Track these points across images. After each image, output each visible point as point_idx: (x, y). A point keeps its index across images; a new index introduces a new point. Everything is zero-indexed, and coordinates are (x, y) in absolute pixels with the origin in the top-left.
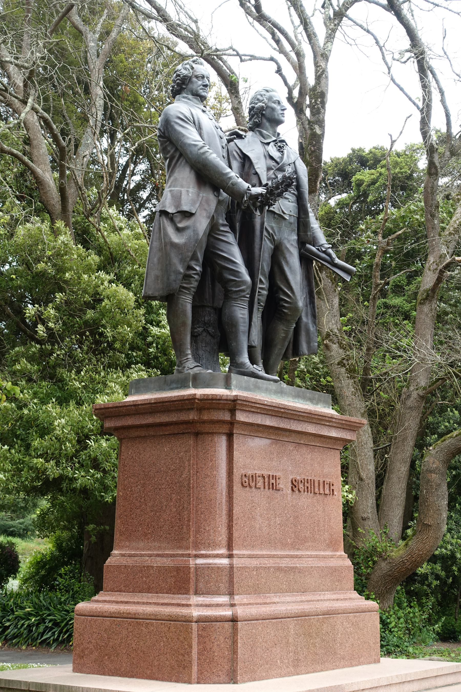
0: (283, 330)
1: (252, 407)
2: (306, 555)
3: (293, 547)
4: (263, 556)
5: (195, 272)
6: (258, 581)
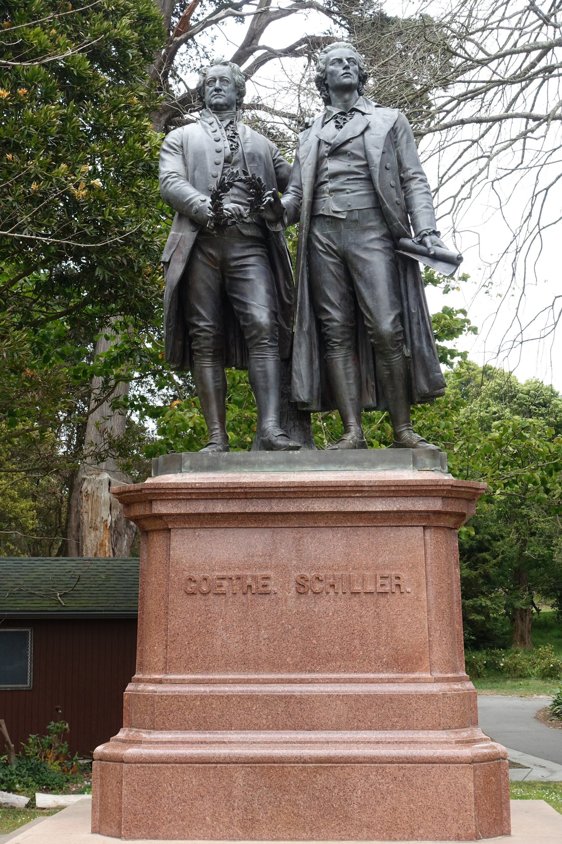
0: (384, 365)
2: (322, 679)
3: (298, 667)
5: (197, 329)
6: (204, 713)
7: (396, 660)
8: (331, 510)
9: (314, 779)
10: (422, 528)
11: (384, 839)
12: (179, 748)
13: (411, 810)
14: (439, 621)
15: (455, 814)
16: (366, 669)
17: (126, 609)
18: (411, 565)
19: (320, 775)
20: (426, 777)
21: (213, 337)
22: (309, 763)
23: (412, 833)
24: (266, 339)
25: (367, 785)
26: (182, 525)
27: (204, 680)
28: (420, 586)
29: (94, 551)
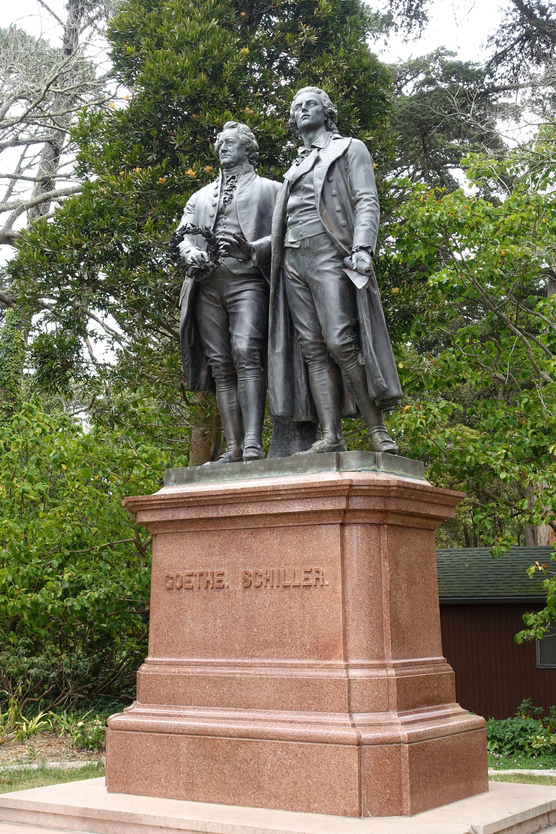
1: (152, 505)
2: (259, 664)
3: (244, 653)
4: (189, 664)
6: (173, 690)
7: (316, 647)
8: (260, 512)
9: (236, 752)
10: (339, 526)
11: (287, 809)
12: (195, 721)
13: (308, 785)
14: (357, 611)
15: (343, 791)
16: (293, 656)
17: (471, 595)
18: (329, 560)
19: (241, 748)
20: (320, 756)
21: (223, 365)
22: (233, 737)
23: (309, 806)
24: (243, 363)
25: (275, 760)
26: (164, 531)
27: (175, 662)
28: (336, 579)
29: (547, 540)
